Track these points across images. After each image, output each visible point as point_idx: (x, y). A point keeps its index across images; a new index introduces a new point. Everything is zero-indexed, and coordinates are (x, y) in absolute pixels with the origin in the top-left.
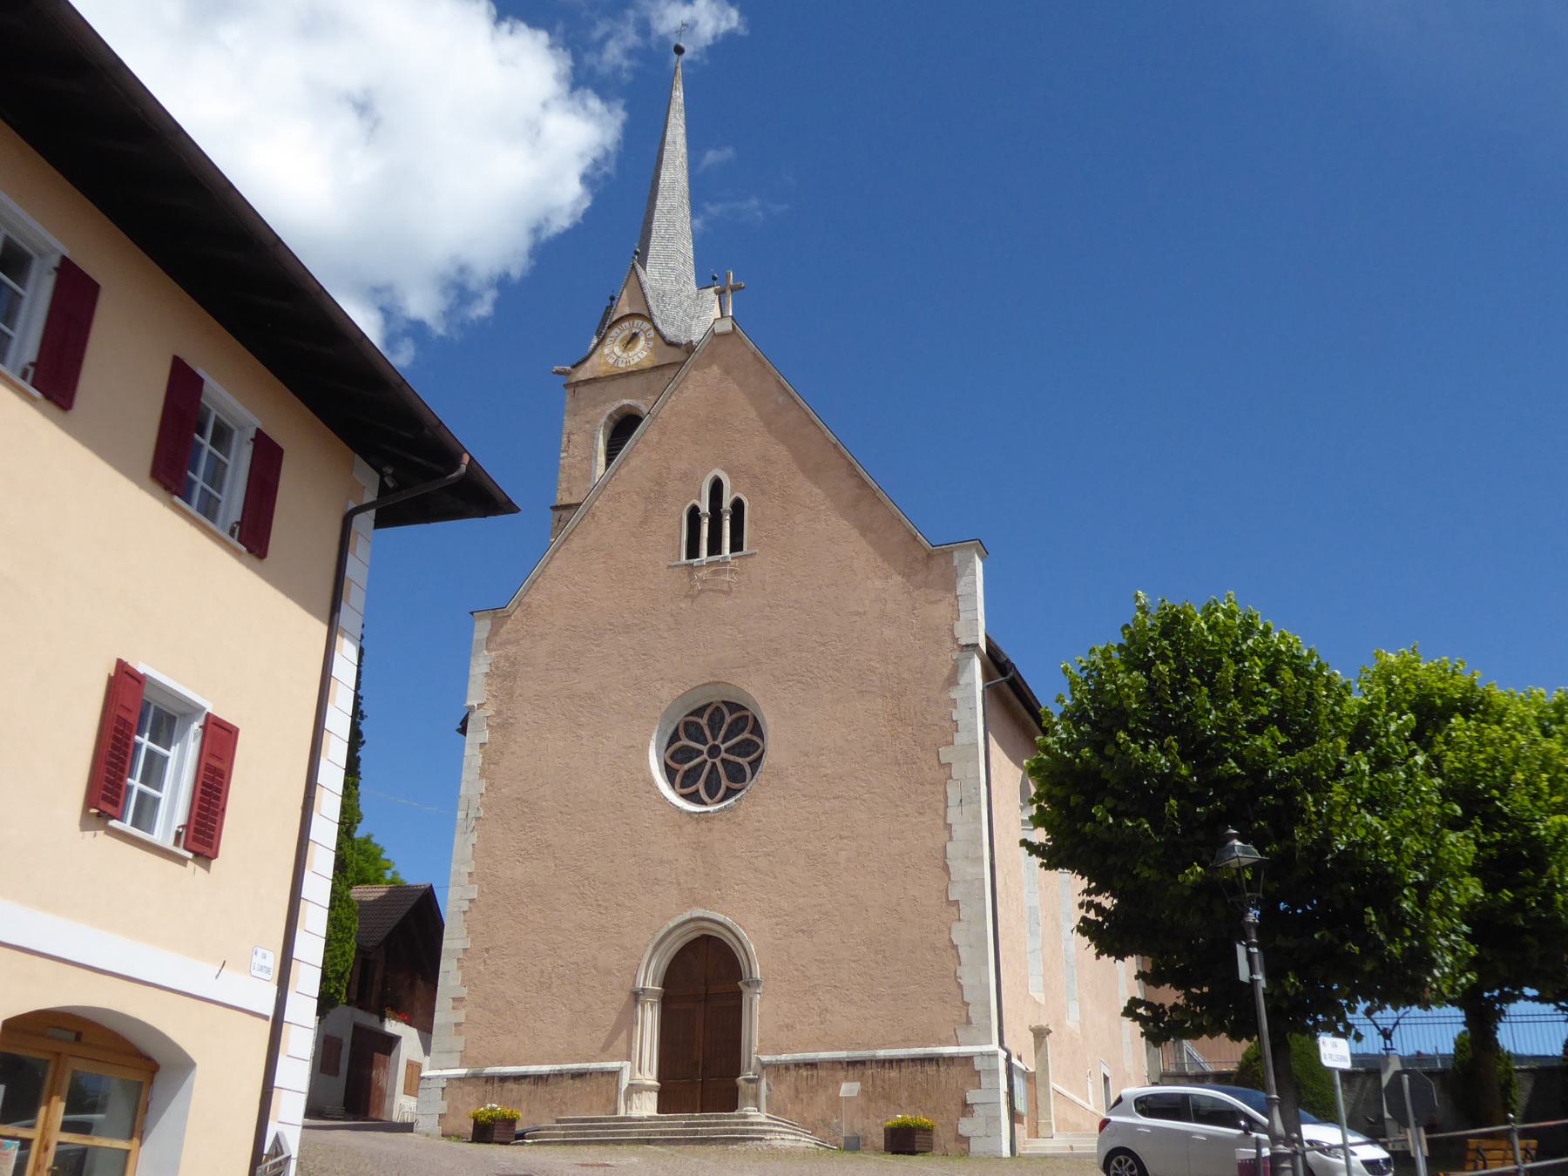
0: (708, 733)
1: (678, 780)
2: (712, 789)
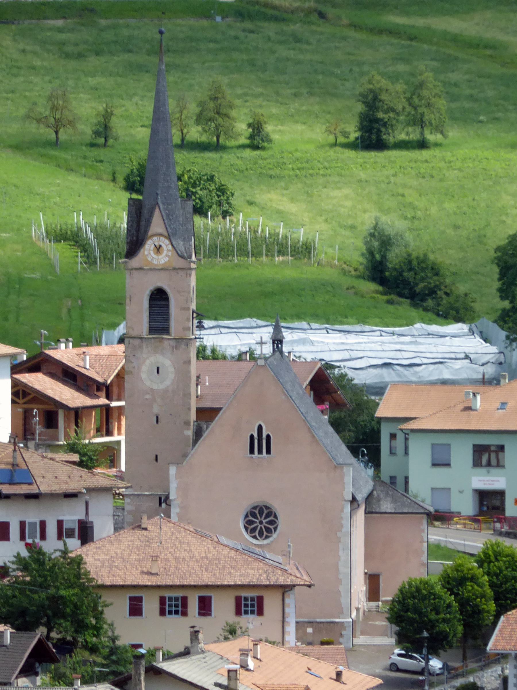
0: (258, 515)
1: (249, 531)
2: (261, 534)
